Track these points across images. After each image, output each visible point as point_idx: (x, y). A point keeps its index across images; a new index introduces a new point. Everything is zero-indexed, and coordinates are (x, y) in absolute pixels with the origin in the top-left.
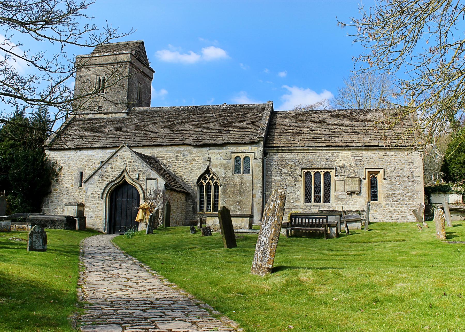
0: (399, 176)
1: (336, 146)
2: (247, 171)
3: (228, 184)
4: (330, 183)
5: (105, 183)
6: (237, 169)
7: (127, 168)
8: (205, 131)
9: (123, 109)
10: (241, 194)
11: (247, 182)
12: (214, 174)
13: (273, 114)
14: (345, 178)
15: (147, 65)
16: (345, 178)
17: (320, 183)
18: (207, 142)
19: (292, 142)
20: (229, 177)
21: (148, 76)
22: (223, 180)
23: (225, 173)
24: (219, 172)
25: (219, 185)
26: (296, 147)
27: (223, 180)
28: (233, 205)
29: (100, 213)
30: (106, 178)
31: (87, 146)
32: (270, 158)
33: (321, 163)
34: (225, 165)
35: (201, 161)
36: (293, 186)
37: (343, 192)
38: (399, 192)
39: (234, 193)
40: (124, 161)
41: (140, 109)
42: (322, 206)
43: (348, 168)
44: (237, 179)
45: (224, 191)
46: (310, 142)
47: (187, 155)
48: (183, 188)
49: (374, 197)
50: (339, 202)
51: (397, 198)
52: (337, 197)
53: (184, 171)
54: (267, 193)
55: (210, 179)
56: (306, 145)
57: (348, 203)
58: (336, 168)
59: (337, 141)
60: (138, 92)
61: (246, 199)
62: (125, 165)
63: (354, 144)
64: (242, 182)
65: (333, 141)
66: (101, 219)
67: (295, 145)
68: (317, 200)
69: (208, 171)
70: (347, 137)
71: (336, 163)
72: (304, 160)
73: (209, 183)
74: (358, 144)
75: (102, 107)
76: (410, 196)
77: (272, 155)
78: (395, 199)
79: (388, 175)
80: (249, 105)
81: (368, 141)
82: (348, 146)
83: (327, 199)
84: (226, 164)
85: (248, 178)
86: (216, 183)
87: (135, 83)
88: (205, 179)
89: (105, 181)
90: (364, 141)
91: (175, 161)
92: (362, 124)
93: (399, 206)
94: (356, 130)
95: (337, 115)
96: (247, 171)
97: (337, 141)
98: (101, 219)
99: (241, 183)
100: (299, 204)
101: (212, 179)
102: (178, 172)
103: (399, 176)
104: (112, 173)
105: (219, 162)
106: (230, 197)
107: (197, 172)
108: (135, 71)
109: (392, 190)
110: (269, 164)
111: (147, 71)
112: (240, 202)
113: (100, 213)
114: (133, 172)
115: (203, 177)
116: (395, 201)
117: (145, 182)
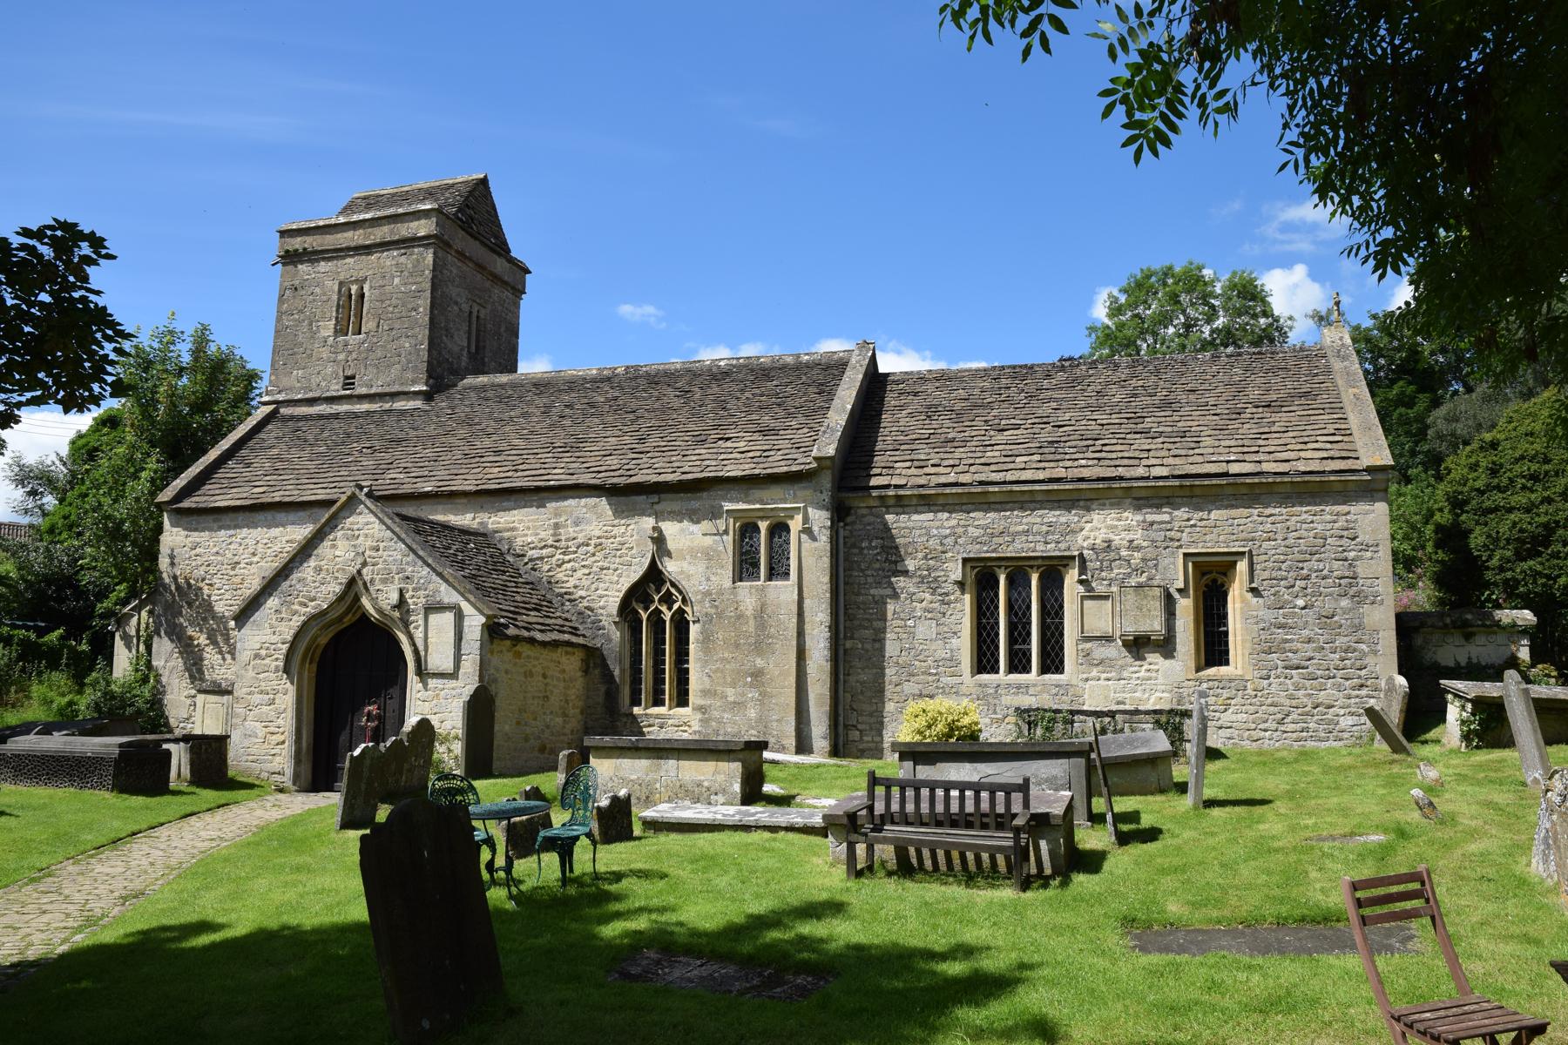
1: (1082, 480)
2: (777, 571)
3: (720, 615)
4: (1061, 607)
5: (297, 622)
6: (745, 566)
7: (364, 571)
8: (652, 442)
9: (414, 382)
11: (778, 606)
12: (673, 584)
13: (875, 384)
14: (1114, 589)
15: (502, 248)
16: (1114, 589)
17: (1029, 607)
18: (615, 480)
19: (933, 470)
20: (721, 593)
21: (506, 283)
23: (708, 579)
24: (689, 577)
25: (690, 618)
26: (945, 485)
27: (701, 602)
29: (281, 722)
32: (858, 527)
33: (1031, 538)
34: (709, 555)
36: (938, 617)
37: (1108, 639)
38: (1306, 633)
39: (737, 646)
41: (482, 379)
42: (1035, 689)
43: (1124, 553)
45: (706, 639)
46: (993, 468)
47: (589, 522)
48: (574, 631)
49: (1214, 650)
50: (1094, 673)
51: (1299, 655)
53: (579, 574)
54: (849, 644)
55: (660, 601)
56: (978, 477)
57: (1125, 674)
58: (1081, 555)
59: (1083, 462)
60: (469, 333)
61: (777, 665)
62: (360, 560)
63: (1141, 471)
64: (763, 605)
65: (1069, 464)
67: (943, 480)
68: (1019, 663)
69: (654, 575)
70: (1119, 448)
71: (1080, 538)
72: (970, 529)
73: (658, 612)
74: (1157, 471)
77: (864, 516)
78: (1294, 659)
79: (1266, 574)
80: (798, 356)
81: (1191, 460)
82: (1121, 478)
83: (1052, 661)
85: (783, 591)
86: (681, 611)
87: (456, 303)
88: (647, 601)
90: (1177, 461)
91: (550, 542)
92: (1166, 404)
93: (1308, 683)
94: (1148, 423)
95: (1084, 377)
97: (1083, 462)
99: (761, 612)
100: (958, 680)
101: (668, 599)
102: (560, 576)
103: (1307, 578)
104: (318, 586)
106: (723, 660)
107: (620, 576)
108: (454, 267)
110: (854, 546)
111: (500, 265)
112: (757, 674)
113: (281, 722)
114: (385, 581)
115: (637, 594)
116: (1291, 668)
117: (421, 616)
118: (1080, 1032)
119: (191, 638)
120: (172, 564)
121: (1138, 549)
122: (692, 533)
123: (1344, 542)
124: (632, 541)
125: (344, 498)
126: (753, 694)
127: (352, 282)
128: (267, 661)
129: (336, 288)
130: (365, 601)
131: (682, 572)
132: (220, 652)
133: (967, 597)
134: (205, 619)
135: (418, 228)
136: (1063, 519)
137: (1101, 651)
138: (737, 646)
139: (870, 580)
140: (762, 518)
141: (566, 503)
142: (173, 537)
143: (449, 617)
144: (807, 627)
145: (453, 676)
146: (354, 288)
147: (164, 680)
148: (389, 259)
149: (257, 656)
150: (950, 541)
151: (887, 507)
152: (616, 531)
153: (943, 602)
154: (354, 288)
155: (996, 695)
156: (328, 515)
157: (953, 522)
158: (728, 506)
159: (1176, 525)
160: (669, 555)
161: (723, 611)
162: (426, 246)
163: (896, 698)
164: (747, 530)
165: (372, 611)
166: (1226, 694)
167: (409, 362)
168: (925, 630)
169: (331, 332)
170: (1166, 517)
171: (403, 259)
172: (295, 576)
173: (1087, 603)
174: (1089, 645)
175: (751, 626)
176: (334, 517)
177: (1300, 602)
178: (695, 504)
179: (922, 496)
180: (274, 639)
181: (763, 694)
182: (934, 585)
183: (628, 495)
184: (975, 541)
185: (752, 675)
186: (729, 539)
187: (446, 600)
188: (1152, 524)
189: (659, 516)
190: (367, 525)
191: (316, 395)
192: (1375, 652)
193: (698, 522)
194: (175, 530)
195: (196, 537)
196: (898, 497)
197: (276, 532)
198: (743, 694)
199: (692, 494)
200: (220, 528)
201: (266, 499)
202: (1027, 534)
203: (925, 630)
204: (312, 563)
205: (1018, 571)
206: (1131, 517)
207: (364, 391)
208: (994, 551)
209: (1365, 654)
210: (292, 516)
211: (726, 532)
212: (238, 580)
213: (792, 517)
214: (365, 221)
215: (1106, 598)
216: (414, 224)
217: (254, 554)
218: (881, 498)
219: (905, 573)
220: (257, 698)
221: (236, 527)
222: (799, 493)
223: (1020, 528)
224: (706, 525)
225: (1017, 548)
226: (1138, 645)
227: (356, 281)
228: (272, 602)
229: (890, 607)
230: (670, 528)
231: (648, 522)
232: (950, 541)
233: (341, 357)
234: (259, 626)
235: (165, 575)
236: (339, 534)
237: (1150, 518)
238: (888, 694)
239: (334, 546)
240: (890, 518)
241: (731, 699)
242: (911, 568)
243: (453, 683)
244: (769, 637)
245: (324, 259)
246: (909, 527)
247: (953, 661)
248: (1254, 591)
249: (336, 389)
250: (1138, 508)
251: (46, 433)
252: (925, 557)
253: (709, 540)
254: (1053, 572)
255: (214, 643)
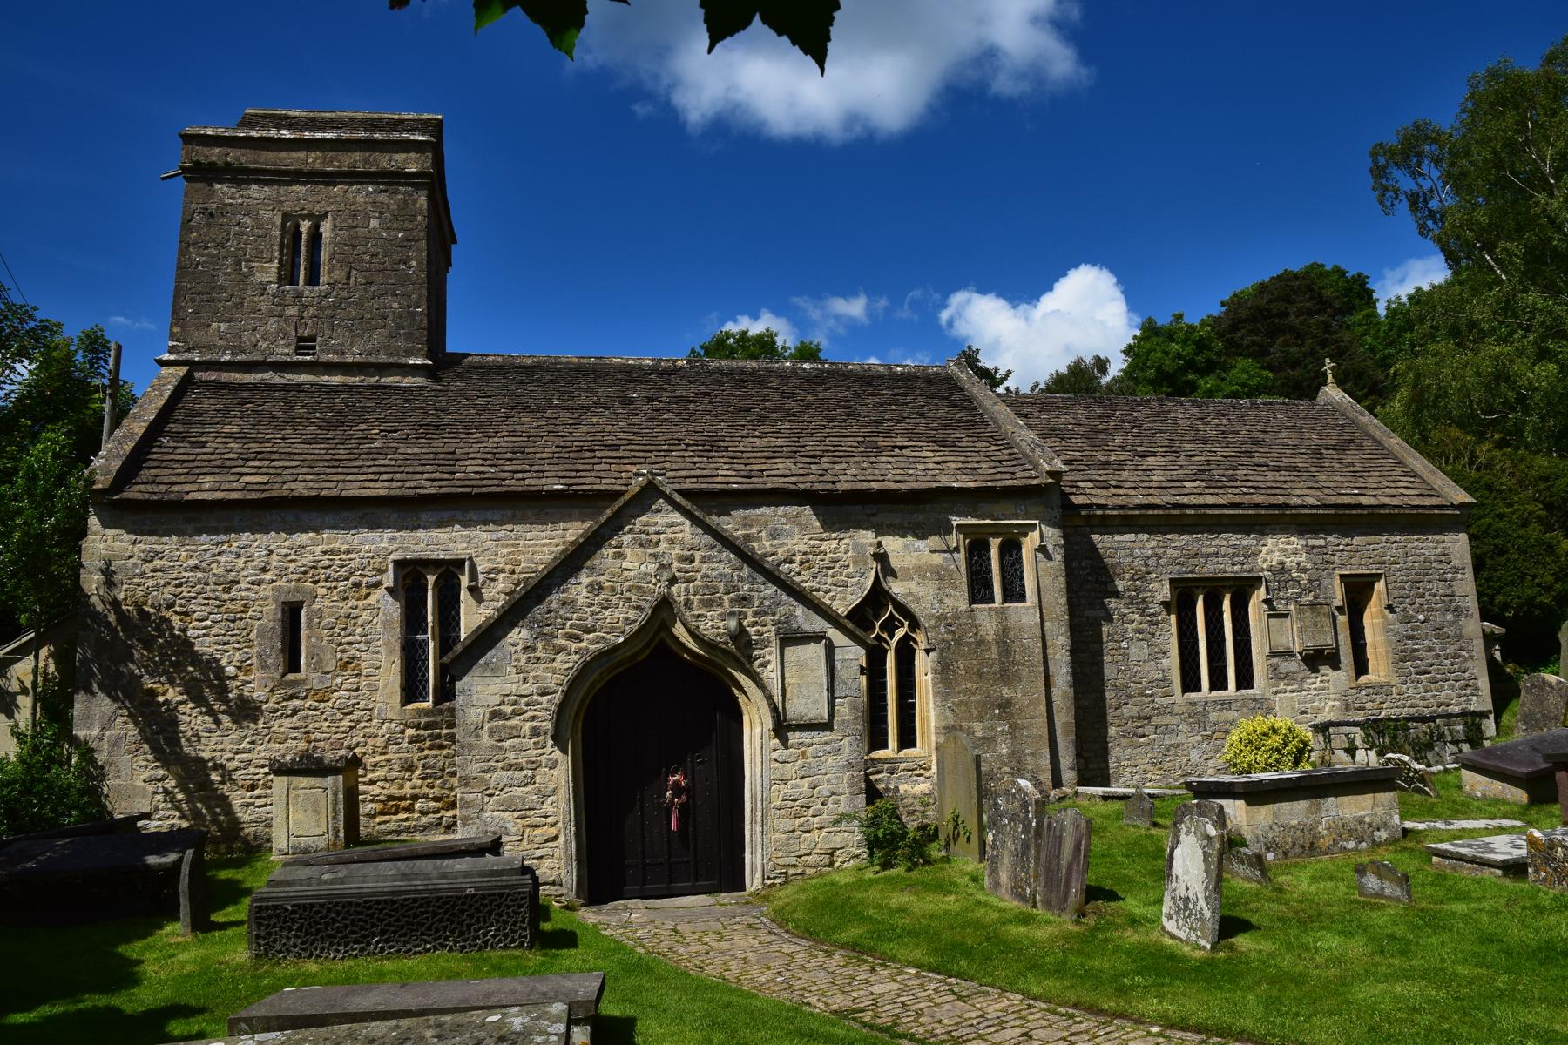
0: (1422, 596)
3: (958, 642)
6: (979, 589)
10: (1006, 675)
11: (1021, 629)
16: (1292, 607)
20: (956, 616)
22: (936, 627)
23: (941, 602)
24: (918, 599)
27: (936, 627)
28: (980, 719)
30: (570, 637)
31: (757, 483)
34: (938, 574)
35: (847, 558)
39: (981, 675)
40: (655, 556)
44: (986, 619)
47: (790, 535)
52: (1275, 669)
61: (1025, 694)
66: (556, 838)
75: (313, 339)
76: (1456, 656)
84: (941, 566)
85: (1025, 614)
89: (563, 649)
96: (1014, 592)
98: (556, 838)
99: (1004, 635)
105: (914, 561)
106: (967, 691)
109: (1411, 638)
112: (1005, 705)
114: (708, 604)
118: (647, 1029)
119: (152, 693)
120: (110, 583)
121: (1304, 570)
122: (918, 550)
123: (1444, 565)
124: (847, 558)
125: (634, 488)
126: (1003, 727)
127: (304, 217)
128: (515, 721)
129: (278, 221)
130: (679, 630)
131: (910, 594)
132: (211, 712)
133: (1173, 618)
134: (179, 666)
135: (406, 162)
136: (1245, 542)
137: (1293, 665)
138: (981, 675)
139: (1083, 601)
140: (995, 535)
141: (758, 511)
142: (103, 543)
143: (816, 651)
144: (1050, 651)
145: (827, 726)
146: (305, 226)
147: (101, 758)
148: (362, 195)
149: (495, 715)
150: (1152, 561)
151: (1091, 527)
152: (825, 546)
153: (1152, 623)
154: (305, 226)
155: (1205, 713)
156: (610, 514)
157: (1153, 543)
158: (956, 521)
159: (1330, 549)
160: (894, 574)
161: (961, 637)
162: (417, 186)
163: (1116, 721)
164: (977, 548)
165: (691, 644)
166: (1379, 699)
167: (400, 327)
168: (1138, 651)
169: (272, 277)
170: (1322, 542)
171: (382, 197)
172: (555, 598)
173: (1272, 621)
174: (1275, 661)
175: (994, 653)
176: (617, 514)
177: (1421, 617)
178: (920, 518)
179: (1126, 516)
180: (527, 688)
181: (1013, 727)
182: (1142, 606)
183: (840, 509)
184: (1173, 561)
185: (999, 707)
186: (961, 556)
187: (806, 627)
188: (1313, 547)
189: (880, 531)
190: (670, 528)
191: (257, 357)
192: (1471, 657)
193: (923, 537)
194: (111, 532)
195: (150, 543)
196: (1104, 516)
197: (304, 538)
198: (992, 729)
199: (914, 510)
200: (199, 533)
201: (513, 485)
202: (1219, 554)
203: (1138, 651)
204: (585, 578)
205: (1213, 590)
206: (1297, 542)
207: (332, 358)
208: (1192, 572)
209: (1466, 660)
210: (329, 518)
211: (957, 549)
212: (238, 605)
213: (1026, 535)
214: (324, 140)
215: (1285, 616)
216: (400, 157)
217: (264, 570)
218: (1088, 517)
219: (1116, 595)
220: (502, 776)
221: (227, 531)
222: (1031, 509)
223: (1212, 550)
224: (934, 541)
225: (1208, 570)
226: (1317, 659)
227: (309, 217)
228: (518, 636)
229: (1105, 629)
230: (892, 544)
231: (867, 537)
232: (1152, 561)
233: (292, 311)
234: (496, 671)
235: (95, 600)
236: (627, 539)
237: (1312, 542)
238: (1110, 719)
239: (619, 556)
240: (1095, 537)
241: (979, 734)
242: (1120, 589)
243: (827, 736)
244: (1014, 663)
245: (257, 182)
246: (1118, 547)
247: (1165, 681)
248: (1390, 608)
249: (284, 352)
250: (1301, 534)
251: (24, 370)
252: (1132, 579)
253: (938, 559)
254: (1242, 589)
255: (199, 700)
